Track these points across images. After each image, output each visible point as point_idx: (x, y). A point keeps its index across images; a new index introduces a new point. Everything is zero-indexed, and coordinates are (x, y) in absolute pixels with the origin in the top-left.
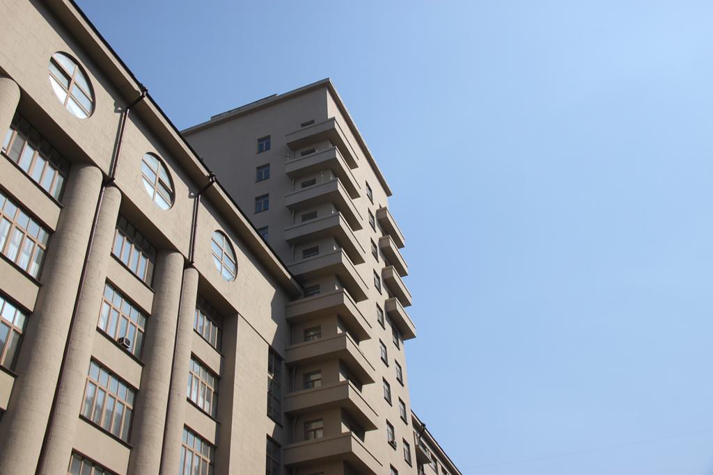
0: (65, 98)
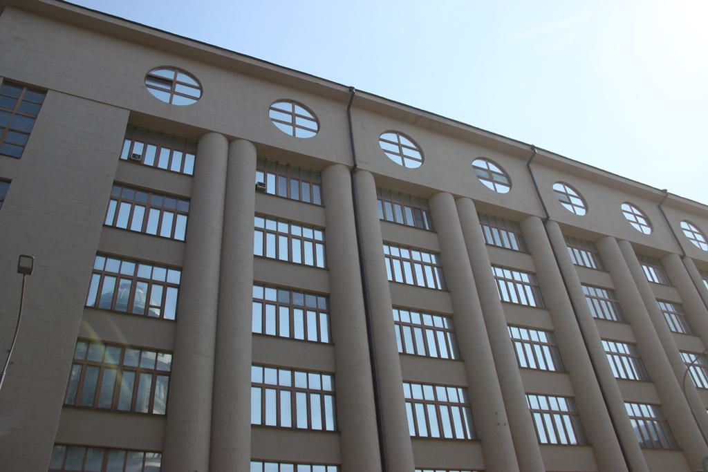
0: (398, 149)
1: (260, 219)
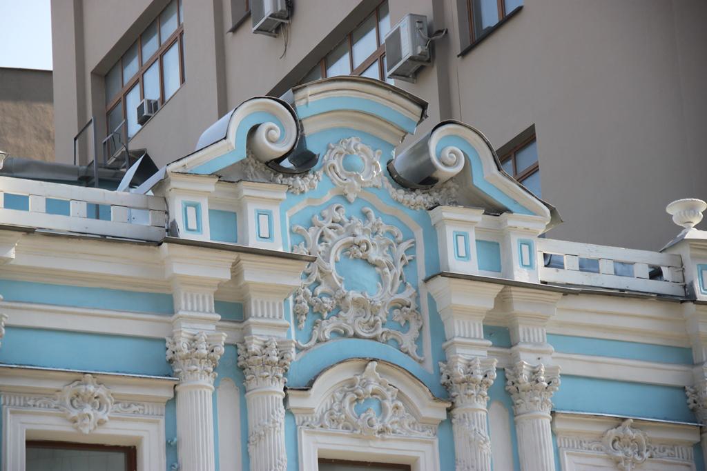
1: (493, 305)
